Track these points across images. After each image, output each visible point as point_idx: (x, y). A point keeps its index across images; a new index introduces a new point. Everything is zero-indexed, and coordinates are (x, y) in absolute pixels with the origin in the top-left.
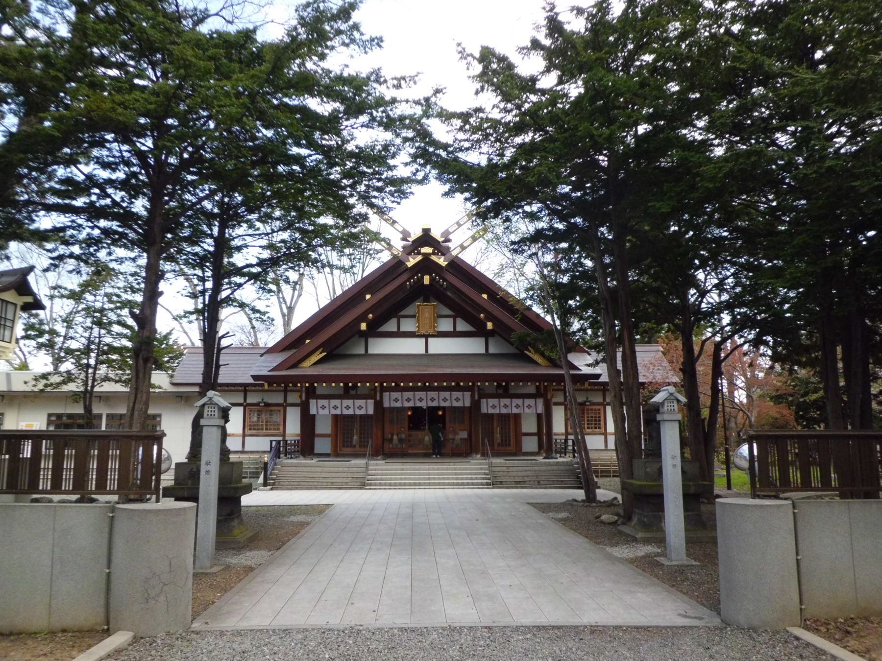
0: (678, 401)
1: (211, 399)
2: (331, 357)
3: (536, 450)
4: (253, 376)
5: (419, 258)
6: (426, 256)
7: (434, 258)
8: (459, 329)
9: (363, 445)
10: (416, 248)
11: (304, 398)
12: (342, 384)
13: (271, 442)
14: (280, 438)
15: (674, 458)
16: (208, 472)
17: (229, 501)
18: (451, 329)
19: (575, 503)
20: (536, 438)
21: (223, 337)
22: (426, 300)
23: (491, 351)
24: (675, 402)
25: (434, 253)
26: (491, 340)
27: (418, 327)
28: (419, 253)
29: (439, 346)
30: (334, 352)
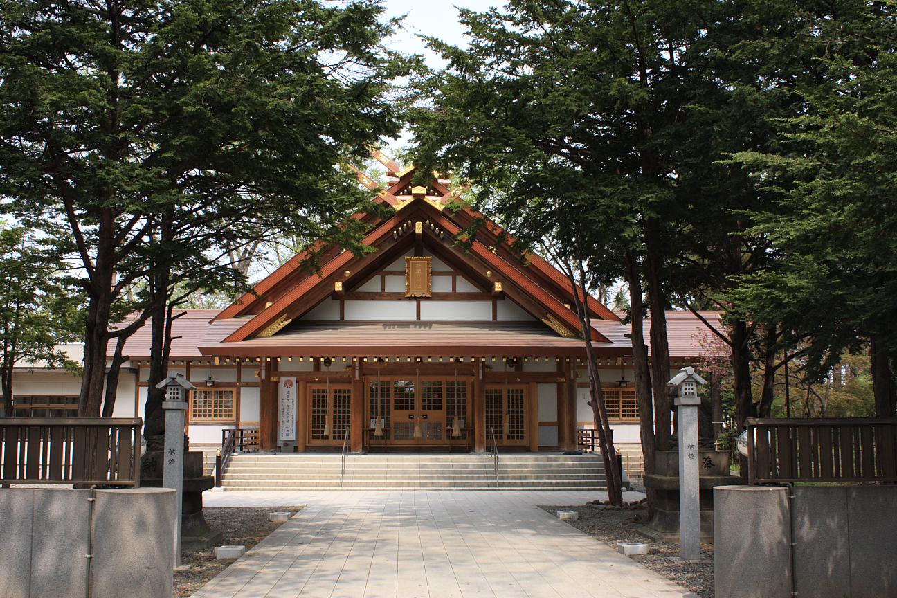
0: (698, 383)
1: (174, 379)
2: (299, 324)
3: (554, 442)
4: (201, 349)
5: (409, 199)
6: (419, 198)
7: (429, 200)
8: (460, 289)
9: (339, 433)
10: (406, 186)
11: (264, 377)
12: (311, 359)
13: (224, 431)
14: (233, 427)
15: (690, 447)
16: (172, 461)
17: (192, 499)
18: (450, 290)
19: (596, 506)
20: (555, 429)
21: (175, 303)
22: (419, 253)
23: (499, 319)
24: (694, 384)
25: (428, 194)
26: (499, 304)
27: (408, 286)
28: (409, 193)
29: (431, 311)
30: (302, 319)
